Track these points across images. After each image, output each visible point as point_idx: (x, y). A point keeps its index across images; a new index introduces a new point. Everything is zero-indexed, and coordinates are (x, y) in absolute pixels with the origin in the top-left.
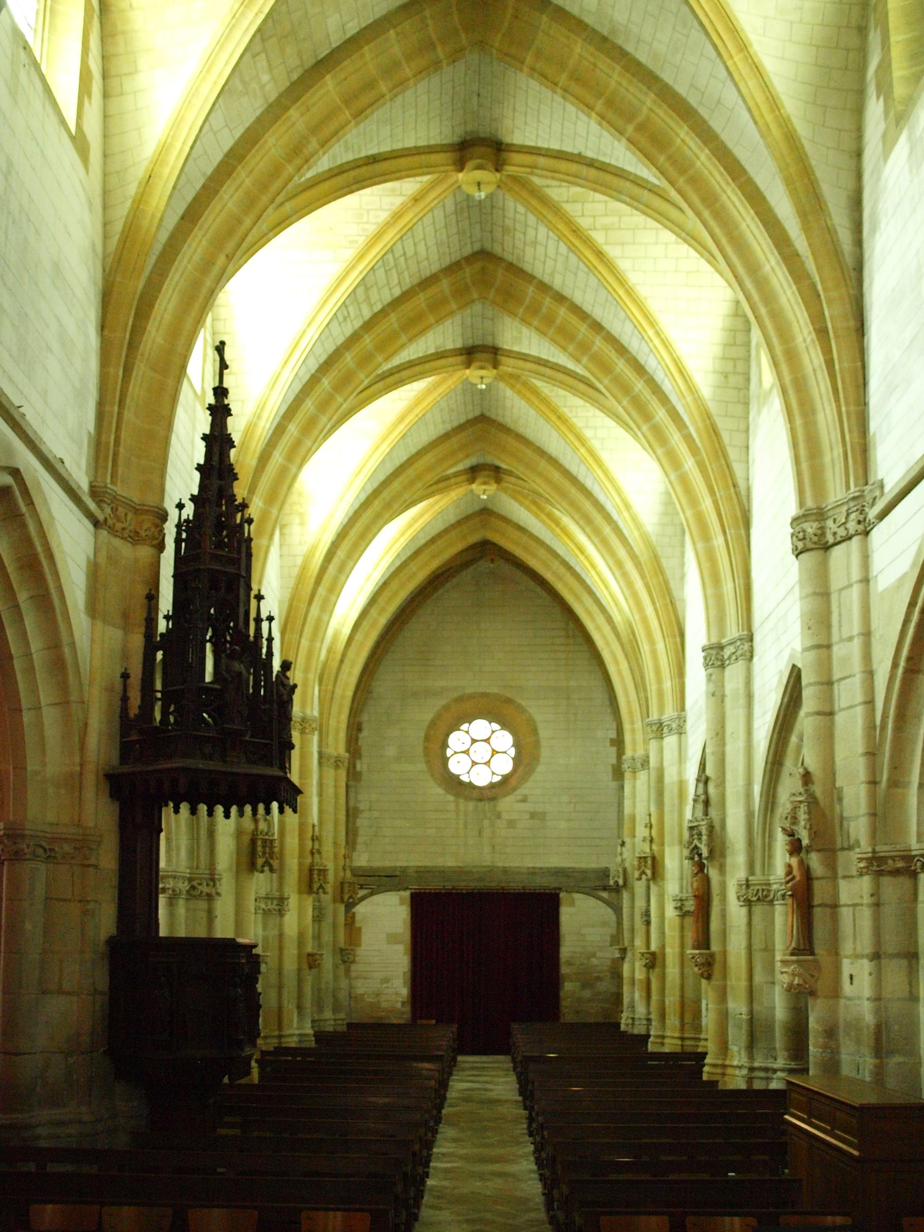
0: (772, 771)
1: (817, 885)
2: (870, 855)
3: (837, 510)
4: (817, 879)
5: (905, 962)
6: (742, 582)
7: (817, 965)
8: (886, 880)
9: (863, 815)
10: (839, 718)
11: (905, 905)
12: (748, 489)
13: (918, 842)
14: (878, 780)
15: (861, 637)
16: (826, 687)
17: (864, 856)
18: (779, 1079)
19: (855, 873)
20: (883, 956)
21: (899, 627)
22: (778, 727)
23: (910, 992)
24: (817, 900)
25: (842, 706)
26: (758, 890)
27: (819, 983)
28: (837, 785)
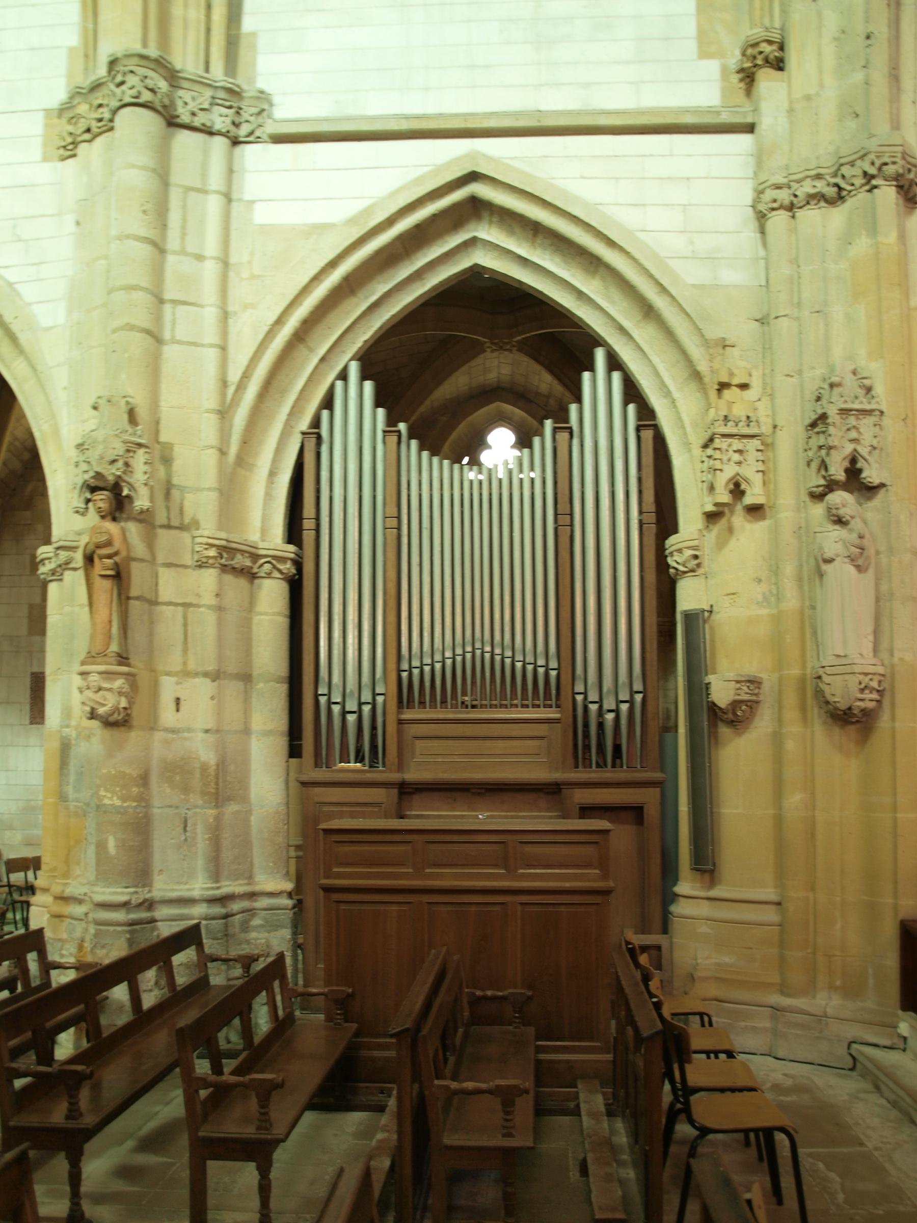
2: (223, 543)
5: (240, 685)
8: (229, 578)
20: (222, 676)
21: (305, 280)
28: (163, 438)
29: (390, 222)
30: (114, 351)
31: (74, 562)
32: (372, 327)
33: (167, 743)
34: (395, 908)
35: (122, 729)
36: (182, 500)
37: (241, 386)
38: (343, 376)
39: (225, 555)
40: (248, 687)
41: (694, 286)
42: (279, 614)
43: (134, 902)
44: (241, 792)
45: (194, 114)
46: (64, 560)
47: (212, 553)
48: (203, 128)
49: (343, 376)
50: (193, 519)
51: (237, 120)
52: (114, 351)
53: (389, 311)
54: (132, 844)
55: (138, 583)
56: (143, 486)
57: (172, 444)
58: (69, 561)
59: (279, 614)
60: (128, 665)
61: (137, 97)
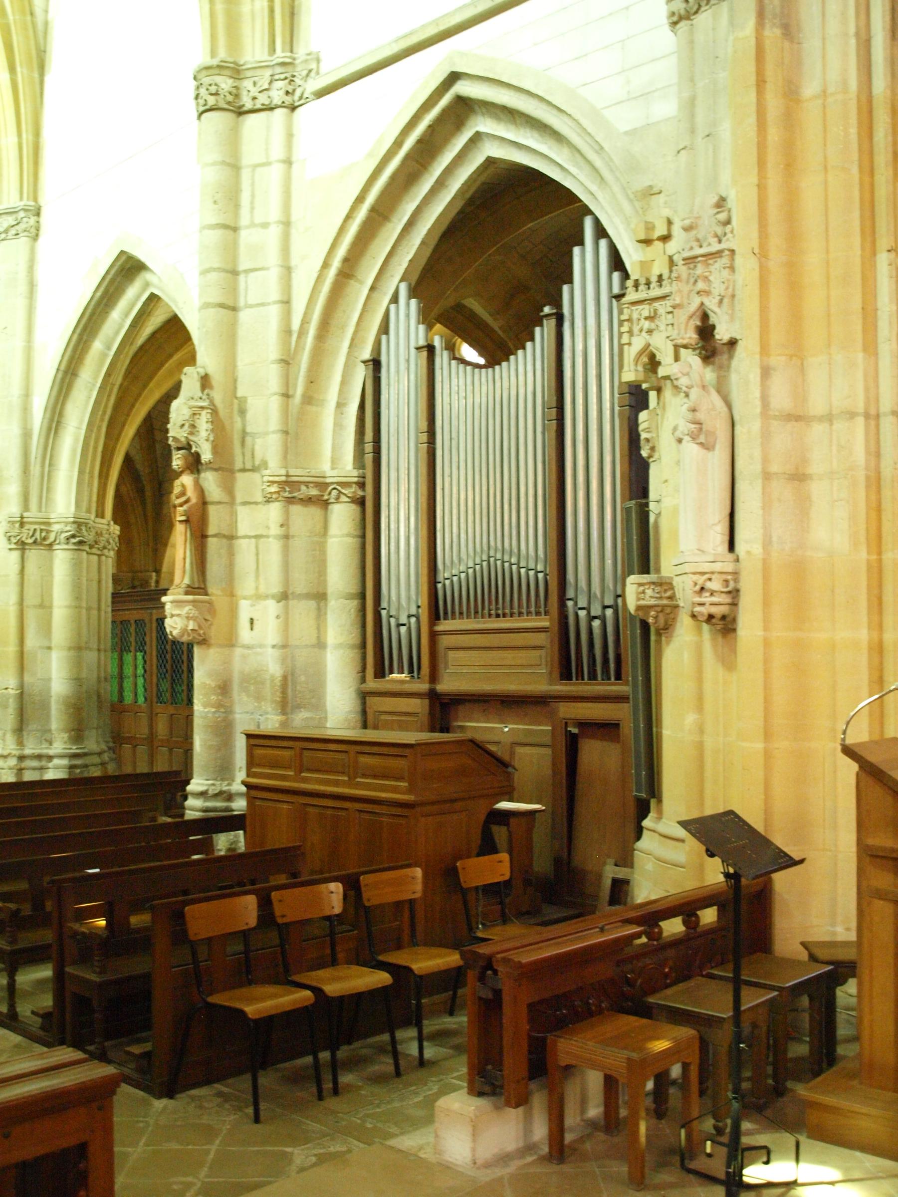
0: (63, 380)
1: (212, 510)
2: (283, 478)
3: (259, 72)
4: (213, 503)
5: (312, 604)
6: (31, 138)
7: (211, 608)
8: (296, 509)
9: (273, 432)
10: (244, 316)
11: (315, 539)
12: (46, 24)
13: (333, 469)
14: (291, 393)
15: (281, 226)
16: (229, 275)
17: (277, 479)
18: (56, 768)
19: (260, 499)
20: (290, 597)
22: (81, 326)
23: (318, 638)
24: (212, 530)
25: (251, 301)
26: (35, 530)
27: (213, 628)
29: (398, 143)
32: (413, 245)
33: (244, 657)
34: (285, 806)
35: (204, 646)
36: (253, 445)
37: (302, 332)
38: (395, 299)
39: (287, 489)
40: (322, 604)
41: (626, 133)
42: (348, 535)
43: (210, 792)
44: (313, 701)
45: (254, 98)
47: (274, 488)
48: (264, 107)
49: (395, 299)
50: (262, 460)
51: (290, 89)
53: (425, 226)
54: (211, 743)
55: (216, 521)
56: (205, 442)
57: (245, 397)
59: (348, 535)
60: (206, 594)
61: (205, 105)
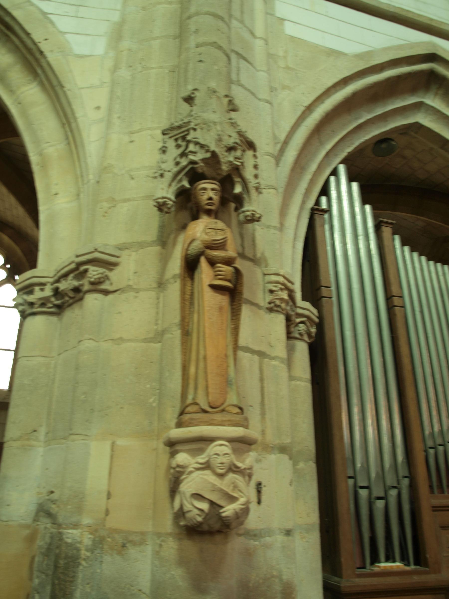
30: (201, 61)
31: (107, 282)
38: (335, 173)
46: (96, 277)
52: (201, 61)
58: (102, 280)
